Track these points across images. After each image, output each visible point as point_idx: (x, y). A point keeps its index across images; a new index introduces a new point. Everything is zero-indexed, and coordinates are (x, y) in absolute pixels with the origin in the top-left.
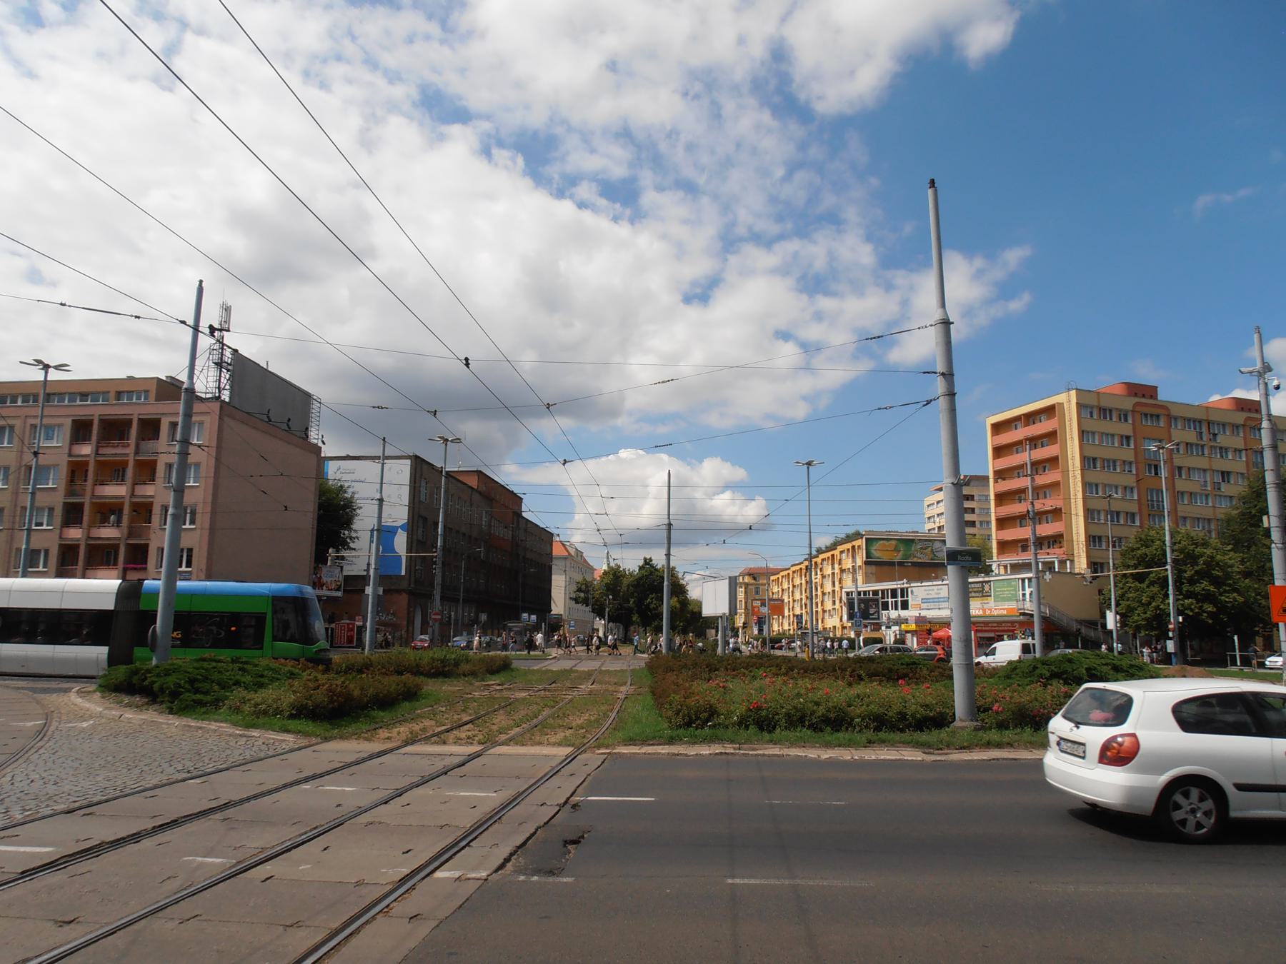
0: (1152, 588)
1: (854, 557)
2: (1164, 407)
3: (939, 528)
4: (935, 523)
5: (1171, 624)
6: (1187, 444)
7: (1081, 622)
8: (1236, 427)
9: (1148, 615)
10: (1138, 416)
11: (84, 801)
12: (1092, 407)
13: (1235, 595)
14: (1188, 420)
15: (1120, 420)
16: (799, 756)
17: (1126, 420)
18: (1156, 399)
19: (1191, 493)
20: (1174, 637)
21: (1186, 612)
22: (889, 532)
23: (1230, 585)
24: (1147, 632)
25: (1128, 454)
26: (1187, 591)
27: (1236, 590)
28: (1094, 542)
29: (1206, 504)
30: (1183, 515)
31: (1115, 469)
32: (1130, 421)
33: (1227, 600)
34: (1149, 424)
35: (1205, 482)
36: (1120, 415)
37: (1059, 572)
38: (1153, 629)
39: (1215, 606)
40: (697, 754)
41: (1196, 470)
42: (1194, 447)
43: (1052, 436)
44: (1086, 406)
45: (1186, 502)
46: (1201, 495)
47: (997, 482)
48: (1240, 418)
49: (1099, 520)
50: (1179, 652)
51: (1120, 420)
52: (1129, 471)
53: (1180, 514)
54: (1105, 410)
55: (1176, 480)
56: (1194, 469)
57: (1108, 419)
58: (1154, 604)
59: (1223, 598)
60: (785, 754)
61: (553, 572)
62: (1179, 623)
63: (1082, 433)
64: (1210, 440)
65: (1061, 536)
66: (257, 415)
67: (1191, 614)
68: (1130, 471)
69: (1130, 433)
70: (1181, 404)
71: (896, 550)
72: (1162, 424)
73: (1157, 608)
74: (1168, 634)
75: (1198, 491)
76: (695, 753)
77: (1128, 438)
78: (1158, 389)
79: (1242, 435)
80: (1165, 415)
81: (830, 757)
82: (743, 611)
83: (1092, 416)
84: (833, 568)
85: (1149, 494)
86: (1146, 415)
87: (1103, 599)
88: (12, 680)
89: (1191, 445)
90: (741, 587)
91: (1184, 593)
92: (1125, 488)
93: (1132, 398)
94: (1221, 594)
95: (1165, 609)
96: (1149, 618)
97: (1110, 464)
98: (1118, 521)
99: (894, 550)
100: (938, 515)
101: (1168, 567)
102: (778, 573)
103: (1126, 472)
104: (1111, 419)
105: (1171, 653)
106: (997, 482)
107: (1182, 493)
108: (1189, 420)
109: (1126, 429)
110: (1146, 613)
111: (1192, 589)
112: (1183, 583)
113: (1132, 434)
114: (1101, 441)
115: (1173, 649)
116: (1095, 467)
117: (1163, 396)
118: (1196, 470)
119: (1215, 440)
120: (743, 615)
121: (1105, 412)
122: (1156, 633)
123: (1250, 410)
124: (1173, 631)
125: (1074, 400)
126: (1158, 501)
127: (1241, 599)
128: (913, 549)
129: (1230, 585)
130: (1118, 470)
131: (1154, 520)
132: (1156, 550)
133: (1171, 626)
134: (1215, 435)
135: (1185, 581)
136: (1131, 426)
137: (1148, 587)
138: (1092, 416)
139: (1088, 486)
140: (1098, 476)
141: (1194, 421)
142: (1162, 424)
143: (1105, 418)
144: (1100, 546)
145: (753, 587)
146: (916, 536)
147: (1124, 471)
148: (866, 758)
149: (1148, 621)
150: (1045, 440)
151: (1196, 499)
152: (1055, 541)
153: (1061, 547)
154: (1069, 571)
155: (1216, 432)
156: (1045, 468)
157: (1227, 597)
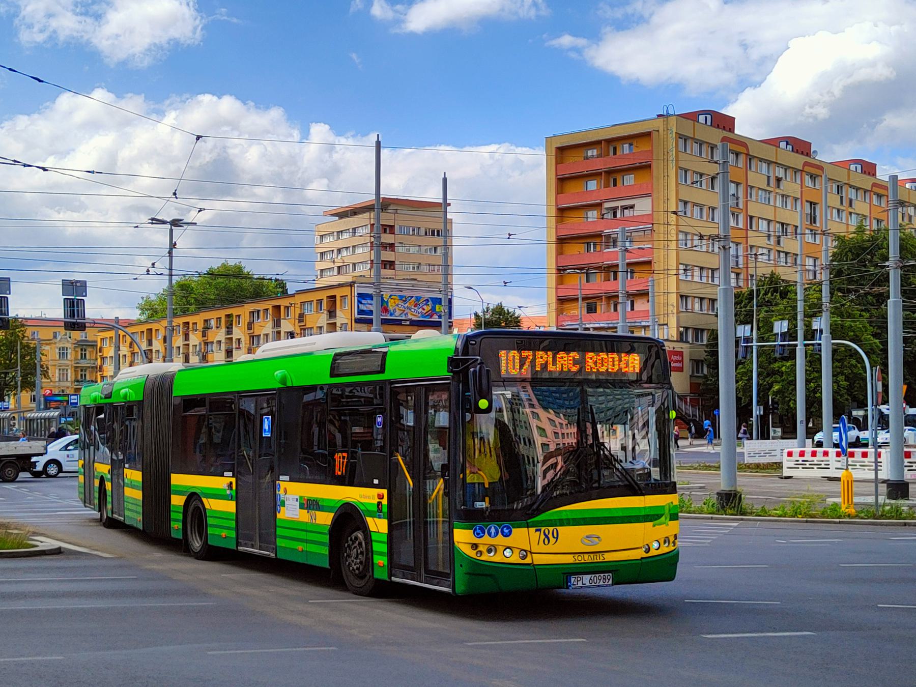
2: (742, 143)
8: (796, 171)
79: (799, 181)
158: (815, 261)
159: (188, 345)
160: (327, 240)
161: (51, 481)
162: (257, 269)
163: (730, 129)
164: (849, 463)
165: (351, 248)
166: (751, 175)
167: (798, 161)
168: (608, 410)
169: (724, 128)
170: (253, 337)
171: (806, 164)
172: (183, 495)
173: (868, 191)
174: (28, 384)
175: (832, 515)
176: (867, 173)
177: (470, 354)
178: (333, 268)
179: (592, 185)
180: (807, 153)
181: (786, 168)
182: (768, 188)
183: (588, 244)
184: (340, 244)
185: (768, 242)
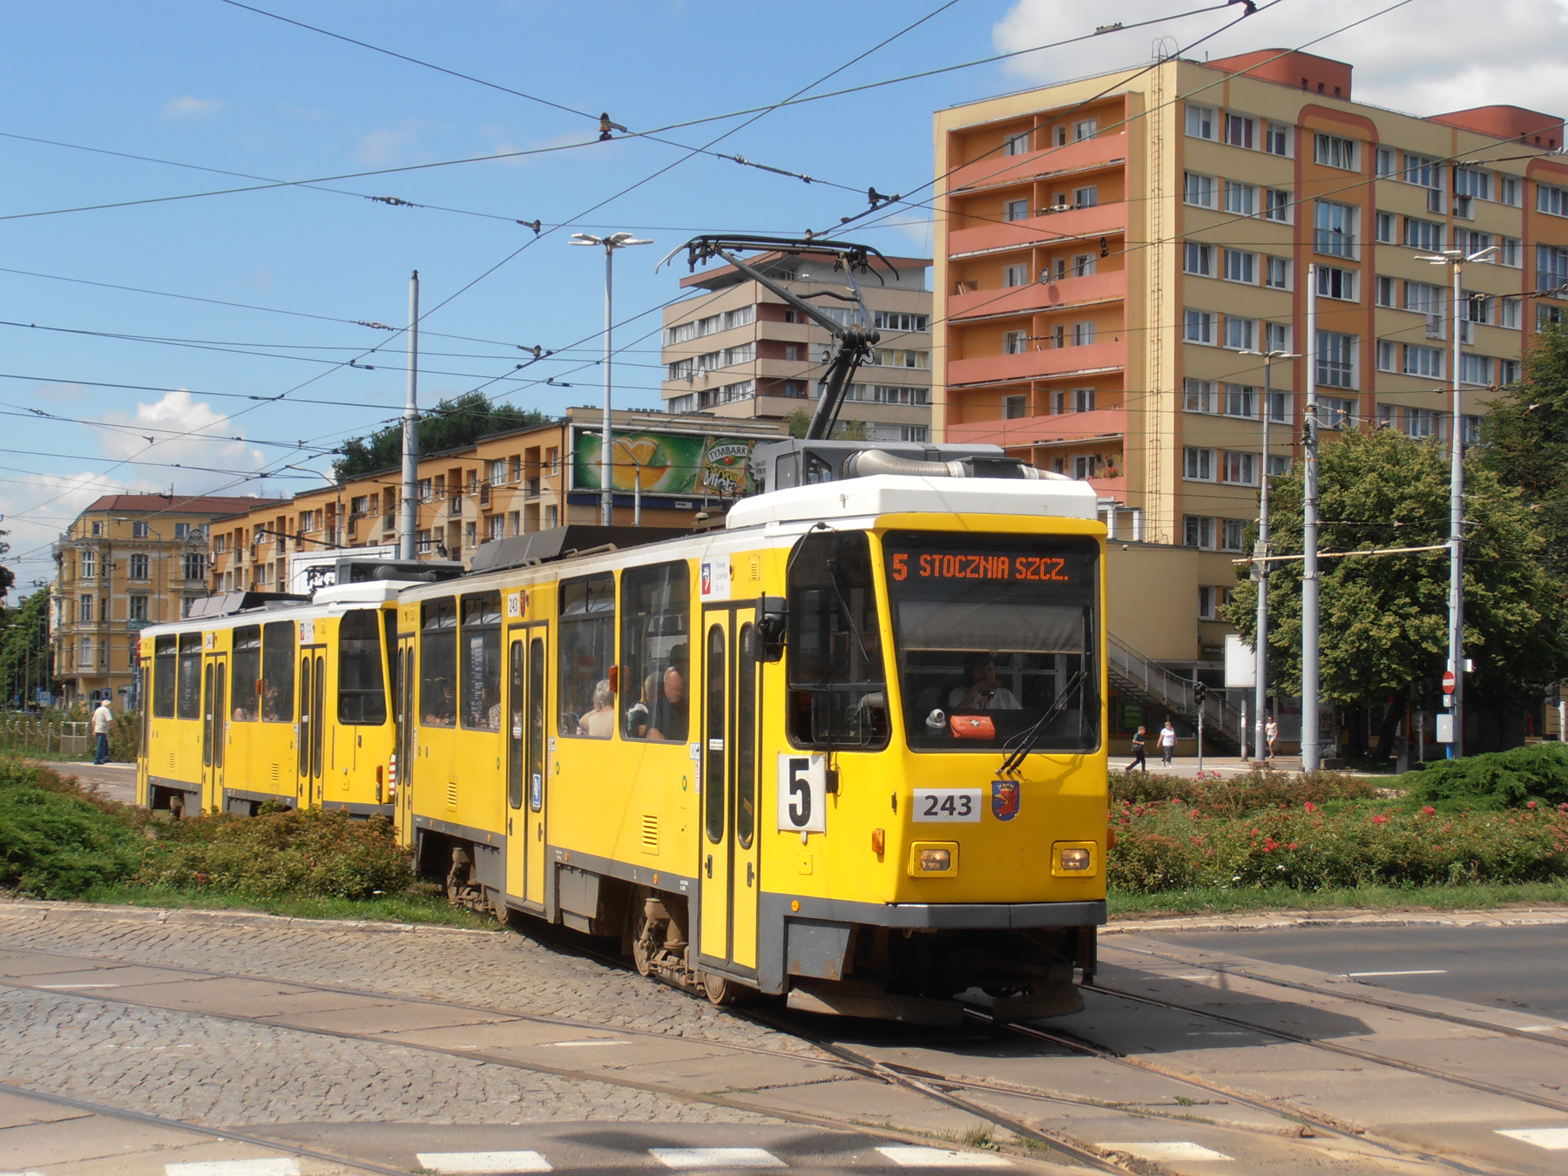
0: (1351, 588)
1: (534, 486)
2: (1365, 120)
3: (704, 395)
4: (691, 381)
5: (1450, 676)
6: (1406, 219)
7: (1159, 668)
8: (1508, 181)
9: (1339, 654)
10: (1307, 140)
12: (1208, 111)
13: (1524, 605)
14: (1411, 158)
15: (1269, 149)
16: (1428, 923)
17: (1281, 150)
18: (1348, 98)
19: (1405, 346)
20: (1452, 708)
21: (1424, 645)
22: (638, 411)
23: (1514, 582)
24: (1335, 695)
25: (1276, 237)
26: (1429, 595)
27: (1524, 594)
28: (1193, 463)
29: (1434, 374)
30: (1386, 400)
31: (1249, 277)
32: (1290, 152)
33: (1510, 617)
34: (1341, 167)
35: (1437, 318)
36: (1269, 135)
37: (1114, 540)
38: (1349, 686)
39: (1483, 632)
40: (1269, 927)
41: (1420, 287)
42: (1215, 187)
43: (1110, 178)
44: (1195, 108)
45: (1393, 369)
46: (1425, 350)
47: (956, 292)
48: (1286, 105)
49: (1207, 405)
50: (1461, 744)
51: (1269, 149)
52: (1278, 284)
53: (1379, 399)
54: (1237, 119)
55: (1376, 311)
56: (1416, 284)
57: (1506, 202)
58: (1356, 627)
59: (1501, 612)
60: (1406, 921)
62: (1465, 674)
63: (1185, 177)
64: (1455, 212)
65: (1116, 446)
67: (1435, 650)
68: (1282, 284)
69: (1515, 231)
70: (1388, 111)
71: (655, 465)
72: (1357, 166)
73: (1364, 635)
74: (1441, 700)
75: (1421, 341)
76: (1266, 925)
77: (1282, 196)
79: (1519, 203)
80: (1363, 142)
81: (1474, 924)
82: (93, 628)
83: (1207, 133)
84: (240, 559)
85: (1329, 347)
86: (1324, 139)
87: (1235, 613)
89: (1415, 221)
90: (89, 555)
91: (1422, 600)
92: (1269, 325)
93: (1300, 93)
94: (1496, 605)
95: (1380, 639)
96: (1343, 660)
97: (1238, 260)
98: (1247, 413)
99: (650, 466)
100: (702, 358)
101: (1452, 545)
102: (245, 515)
103: (1273, 286)
104: (1249, 143)
105: (1444, 745)
106: (956, 292)
107: (1388, 345)
108: (1414, 158)
109: (1278, 172)
110: (1334, 647)
111: (1439, 590)
112: (1421, 577)
113: (1290, 188)
114: (1224, 202)
116: (1205, 270)
117: (1360, 94)
118: (1420, 287)
119: (1464, 213)
120: (94, 639)
121: (1238, 126)
122: (1355, 696)
123: (1321, 89)
124: (1452, 694)
125: (1171, 92)
126: (1335, 364)
127: (1535, 616)
128: (699, 461)
129: (1514, 582)
130: (1256, 280)
132: (1367, 494)
133: (1447, 683)
134: (1465, 200)
135: (1423, 571)
136: (1290, 167)
137: (1343, 584)
138: (1207, 133)
139: (1190, 320)
140: (1216, 294)
141: (1425, 161)
142: (1357, 166)
143: (1236, 141)
144: (1206, 475)
145: (125, 555)
146: (702, 426)
147: (1269, 282)
148: (1524, 923)
149: (1340, 668)
150: (1088, 191)
151: (1414, 361)
152: (1099, 460)
153: (1113, 475)
154: (1136, 538)
155: (1468, 194)
156: (1082, 261)
157: (1508, 610)
159: (240, 569)
160: (683, 335)
162: (498, 398)
165: (722, 355)
166: (1381, 188)
168: (133, 698)
175: (289, 1028)
177: (905, 611)
178: (692, 395)
180: (1338, 90)
183: (1012, 338)
184: (706, 346)
185: (1432, 335)
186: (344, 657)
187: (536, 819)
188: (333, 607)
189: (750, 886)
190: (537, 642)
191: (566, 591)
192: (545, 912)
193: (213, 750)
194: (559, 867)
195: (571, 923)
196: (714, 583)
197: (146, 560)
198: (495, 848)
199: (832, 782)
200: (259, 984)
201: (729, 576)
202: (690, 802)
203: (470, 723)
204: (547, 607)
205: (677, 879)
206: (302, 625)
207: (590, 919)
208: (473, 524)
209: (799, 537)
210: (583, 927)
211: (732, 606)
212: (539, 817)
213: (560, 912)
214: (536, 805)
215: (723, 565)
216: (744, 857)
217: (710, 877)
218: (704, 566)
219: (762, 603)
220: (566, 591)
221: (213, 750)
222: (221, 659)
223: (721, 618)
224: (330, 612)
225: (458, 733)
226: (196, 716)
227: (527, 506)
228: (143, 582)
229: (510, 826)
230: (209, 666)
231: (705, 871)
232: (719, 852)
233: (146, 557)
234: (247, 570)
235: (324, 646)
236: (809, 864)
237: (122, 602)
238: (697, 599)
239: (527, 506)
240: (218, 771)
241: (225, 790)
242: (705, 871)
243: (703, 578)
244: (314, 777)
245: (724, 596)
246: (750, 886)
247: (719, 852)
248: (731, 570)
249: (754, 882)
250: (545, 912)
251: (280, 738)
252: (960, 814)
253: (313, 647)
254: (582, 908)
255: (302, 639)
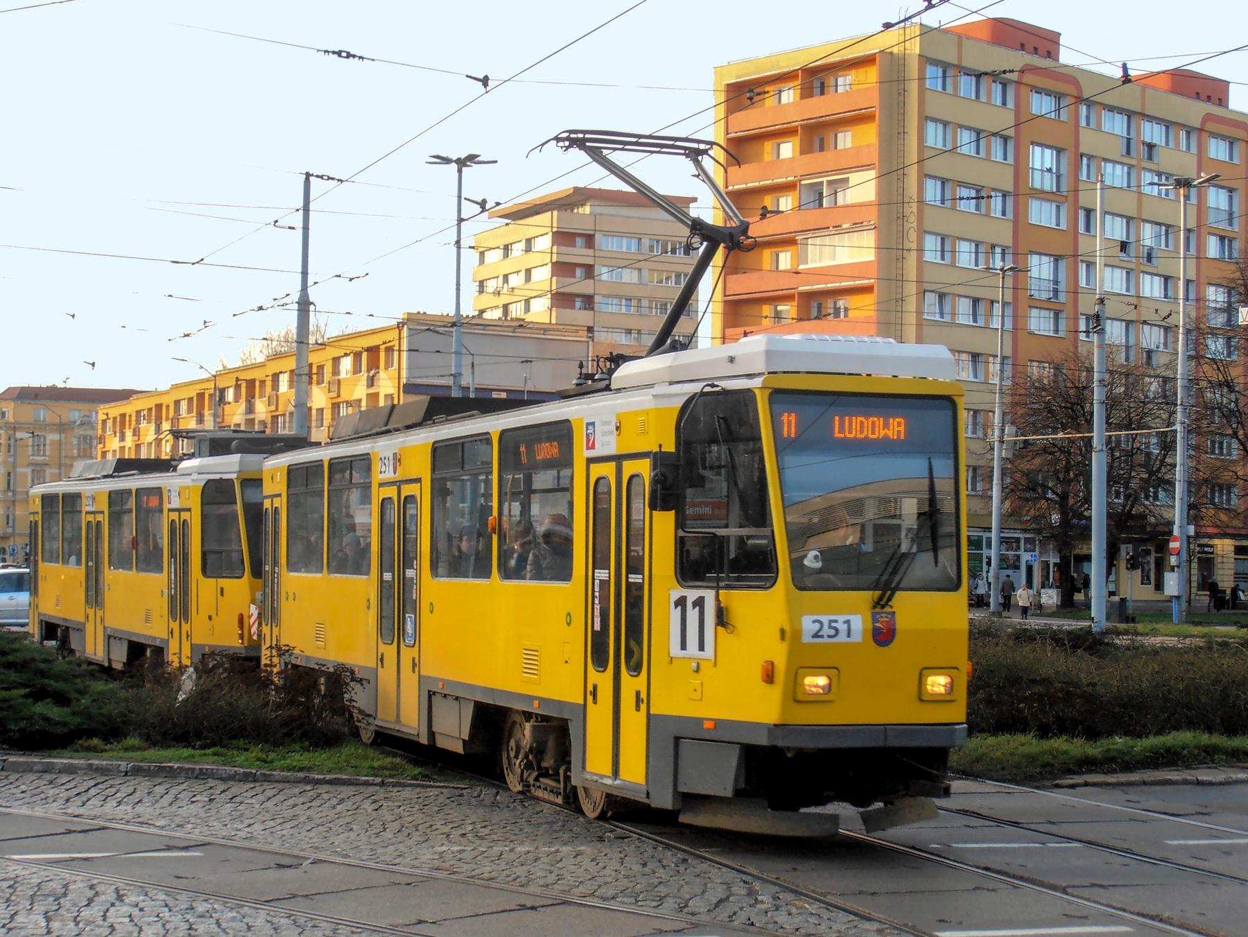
2: (1072, 78)
5: (1176, 539)
11: (750, 870)
18: (1057, 60)
55: (1080, 237)
61: (532, 501)
66: (866, 308)
78: (1061, 37)
84: (122, 439)
88: (381, 727)
115: (1176, 588)
117: (1066, 57)
131: (990, 314)
133: (1174, 545)
158: (977, 246)
161: (60, 618)
163: (1049, 52)
164: (182, 513)
167: (1195, 111)
169: (1209, 98)
170: (338, 404)
171: (1208, 118)
172: (464, 748)
173: (1194, 129)
174: (86, 454)
176: (1203, 96)
179: (788, 149)
180: (1049, 52)
181: (1168, 125)
182: (1126, 160)
186: (204, 517)
187: (407, 654)
188: (195, 476)
189: (414, 672)
190: (410, 499)
191: (292, 471)
192: (418, 734)
193: (94, 593)
194: (109, 637)
195: (442, 743)
196: (599, 439)
197: (45, 440)
198: (80, 629)
199: (722, 618)
200: (250, 853)
201: (615, 433)
202: (575, 643)
203: (63, 563)
204: (421, 466)
205: (560, 704)
206: (169, 491)
207: (464, 741)
208: (322, 410)
209: (684, 399)
210: (458, 748)
211: (618, 459)
212: (640, 683)
213: (432, 735)
214: (409, 641)
215: (608, 423)
216: (631, 685)
217: (383, 667)
218: (588, 424)
219: (659, 459)
220: (440, 452)
221: (94, 593)
222: (185, 515)
223: (608, 470)
224: (193, 480)
225: (58, 566)
226: (564, 574)
227: (368, 395)
228: (42, 458)
229: (87, 617)
230: (385, 502)
231: (590, 698)
232: (604, 681)
233: (45, 438)
234: (130, 448)
235: (189, 510)
236: (699, 690)
237: (25, 474)
238: (581, 454)
239: (246, 420)
240: (186, 627)
241: (652, 721)
242: (590, 698)
243: (588, 435)
244: (274, 627)
245: (612, 450)
246: (414, 672)
247: (604, 681)
248: (617, 428)
249: (643, 707)
250: (418, 734)
251: (157, 583)
252: (829, 636)
253: (179, 510)
254: (119, 657)
255: (170, 503)
